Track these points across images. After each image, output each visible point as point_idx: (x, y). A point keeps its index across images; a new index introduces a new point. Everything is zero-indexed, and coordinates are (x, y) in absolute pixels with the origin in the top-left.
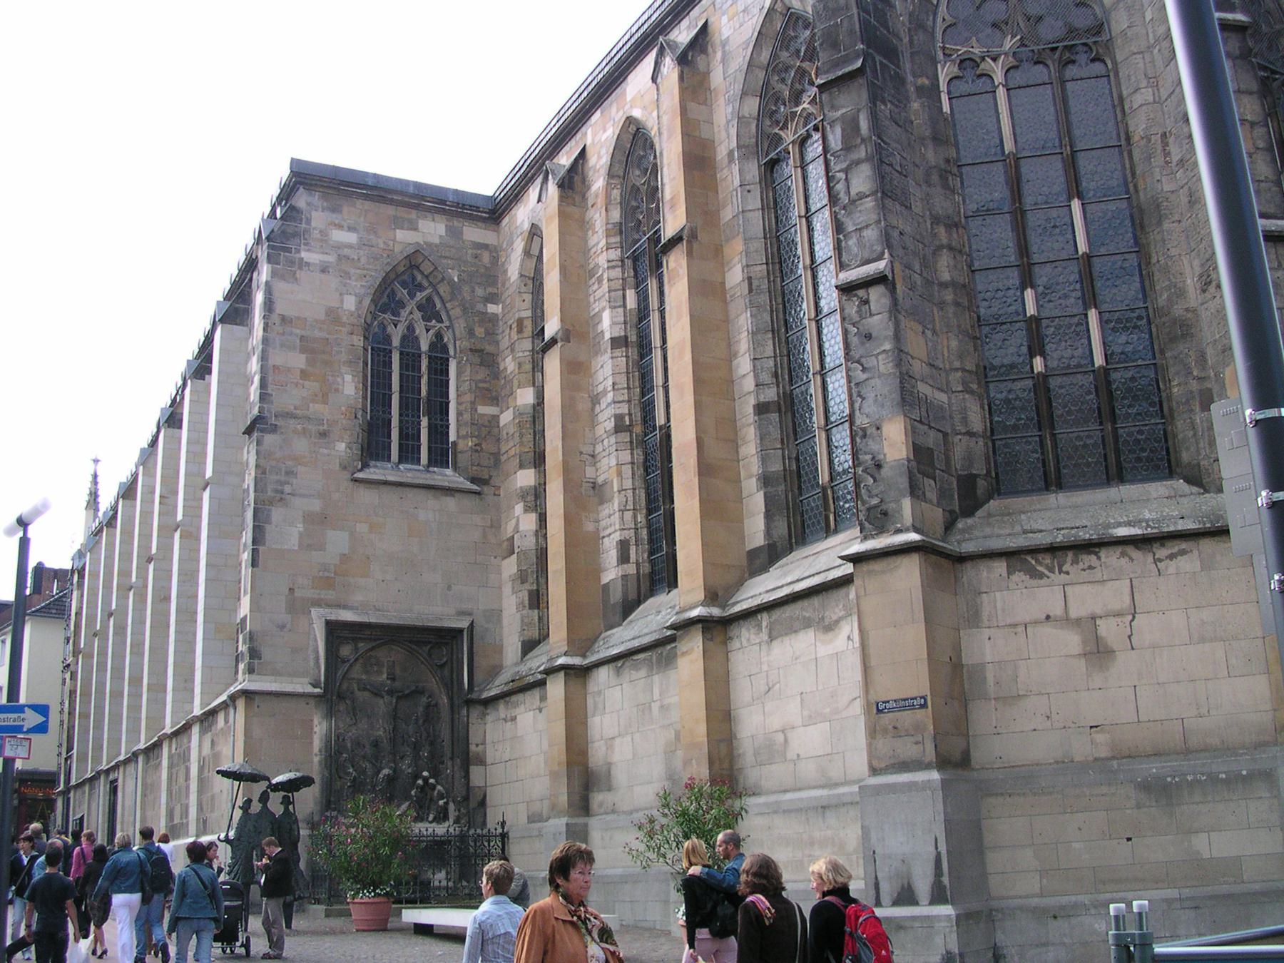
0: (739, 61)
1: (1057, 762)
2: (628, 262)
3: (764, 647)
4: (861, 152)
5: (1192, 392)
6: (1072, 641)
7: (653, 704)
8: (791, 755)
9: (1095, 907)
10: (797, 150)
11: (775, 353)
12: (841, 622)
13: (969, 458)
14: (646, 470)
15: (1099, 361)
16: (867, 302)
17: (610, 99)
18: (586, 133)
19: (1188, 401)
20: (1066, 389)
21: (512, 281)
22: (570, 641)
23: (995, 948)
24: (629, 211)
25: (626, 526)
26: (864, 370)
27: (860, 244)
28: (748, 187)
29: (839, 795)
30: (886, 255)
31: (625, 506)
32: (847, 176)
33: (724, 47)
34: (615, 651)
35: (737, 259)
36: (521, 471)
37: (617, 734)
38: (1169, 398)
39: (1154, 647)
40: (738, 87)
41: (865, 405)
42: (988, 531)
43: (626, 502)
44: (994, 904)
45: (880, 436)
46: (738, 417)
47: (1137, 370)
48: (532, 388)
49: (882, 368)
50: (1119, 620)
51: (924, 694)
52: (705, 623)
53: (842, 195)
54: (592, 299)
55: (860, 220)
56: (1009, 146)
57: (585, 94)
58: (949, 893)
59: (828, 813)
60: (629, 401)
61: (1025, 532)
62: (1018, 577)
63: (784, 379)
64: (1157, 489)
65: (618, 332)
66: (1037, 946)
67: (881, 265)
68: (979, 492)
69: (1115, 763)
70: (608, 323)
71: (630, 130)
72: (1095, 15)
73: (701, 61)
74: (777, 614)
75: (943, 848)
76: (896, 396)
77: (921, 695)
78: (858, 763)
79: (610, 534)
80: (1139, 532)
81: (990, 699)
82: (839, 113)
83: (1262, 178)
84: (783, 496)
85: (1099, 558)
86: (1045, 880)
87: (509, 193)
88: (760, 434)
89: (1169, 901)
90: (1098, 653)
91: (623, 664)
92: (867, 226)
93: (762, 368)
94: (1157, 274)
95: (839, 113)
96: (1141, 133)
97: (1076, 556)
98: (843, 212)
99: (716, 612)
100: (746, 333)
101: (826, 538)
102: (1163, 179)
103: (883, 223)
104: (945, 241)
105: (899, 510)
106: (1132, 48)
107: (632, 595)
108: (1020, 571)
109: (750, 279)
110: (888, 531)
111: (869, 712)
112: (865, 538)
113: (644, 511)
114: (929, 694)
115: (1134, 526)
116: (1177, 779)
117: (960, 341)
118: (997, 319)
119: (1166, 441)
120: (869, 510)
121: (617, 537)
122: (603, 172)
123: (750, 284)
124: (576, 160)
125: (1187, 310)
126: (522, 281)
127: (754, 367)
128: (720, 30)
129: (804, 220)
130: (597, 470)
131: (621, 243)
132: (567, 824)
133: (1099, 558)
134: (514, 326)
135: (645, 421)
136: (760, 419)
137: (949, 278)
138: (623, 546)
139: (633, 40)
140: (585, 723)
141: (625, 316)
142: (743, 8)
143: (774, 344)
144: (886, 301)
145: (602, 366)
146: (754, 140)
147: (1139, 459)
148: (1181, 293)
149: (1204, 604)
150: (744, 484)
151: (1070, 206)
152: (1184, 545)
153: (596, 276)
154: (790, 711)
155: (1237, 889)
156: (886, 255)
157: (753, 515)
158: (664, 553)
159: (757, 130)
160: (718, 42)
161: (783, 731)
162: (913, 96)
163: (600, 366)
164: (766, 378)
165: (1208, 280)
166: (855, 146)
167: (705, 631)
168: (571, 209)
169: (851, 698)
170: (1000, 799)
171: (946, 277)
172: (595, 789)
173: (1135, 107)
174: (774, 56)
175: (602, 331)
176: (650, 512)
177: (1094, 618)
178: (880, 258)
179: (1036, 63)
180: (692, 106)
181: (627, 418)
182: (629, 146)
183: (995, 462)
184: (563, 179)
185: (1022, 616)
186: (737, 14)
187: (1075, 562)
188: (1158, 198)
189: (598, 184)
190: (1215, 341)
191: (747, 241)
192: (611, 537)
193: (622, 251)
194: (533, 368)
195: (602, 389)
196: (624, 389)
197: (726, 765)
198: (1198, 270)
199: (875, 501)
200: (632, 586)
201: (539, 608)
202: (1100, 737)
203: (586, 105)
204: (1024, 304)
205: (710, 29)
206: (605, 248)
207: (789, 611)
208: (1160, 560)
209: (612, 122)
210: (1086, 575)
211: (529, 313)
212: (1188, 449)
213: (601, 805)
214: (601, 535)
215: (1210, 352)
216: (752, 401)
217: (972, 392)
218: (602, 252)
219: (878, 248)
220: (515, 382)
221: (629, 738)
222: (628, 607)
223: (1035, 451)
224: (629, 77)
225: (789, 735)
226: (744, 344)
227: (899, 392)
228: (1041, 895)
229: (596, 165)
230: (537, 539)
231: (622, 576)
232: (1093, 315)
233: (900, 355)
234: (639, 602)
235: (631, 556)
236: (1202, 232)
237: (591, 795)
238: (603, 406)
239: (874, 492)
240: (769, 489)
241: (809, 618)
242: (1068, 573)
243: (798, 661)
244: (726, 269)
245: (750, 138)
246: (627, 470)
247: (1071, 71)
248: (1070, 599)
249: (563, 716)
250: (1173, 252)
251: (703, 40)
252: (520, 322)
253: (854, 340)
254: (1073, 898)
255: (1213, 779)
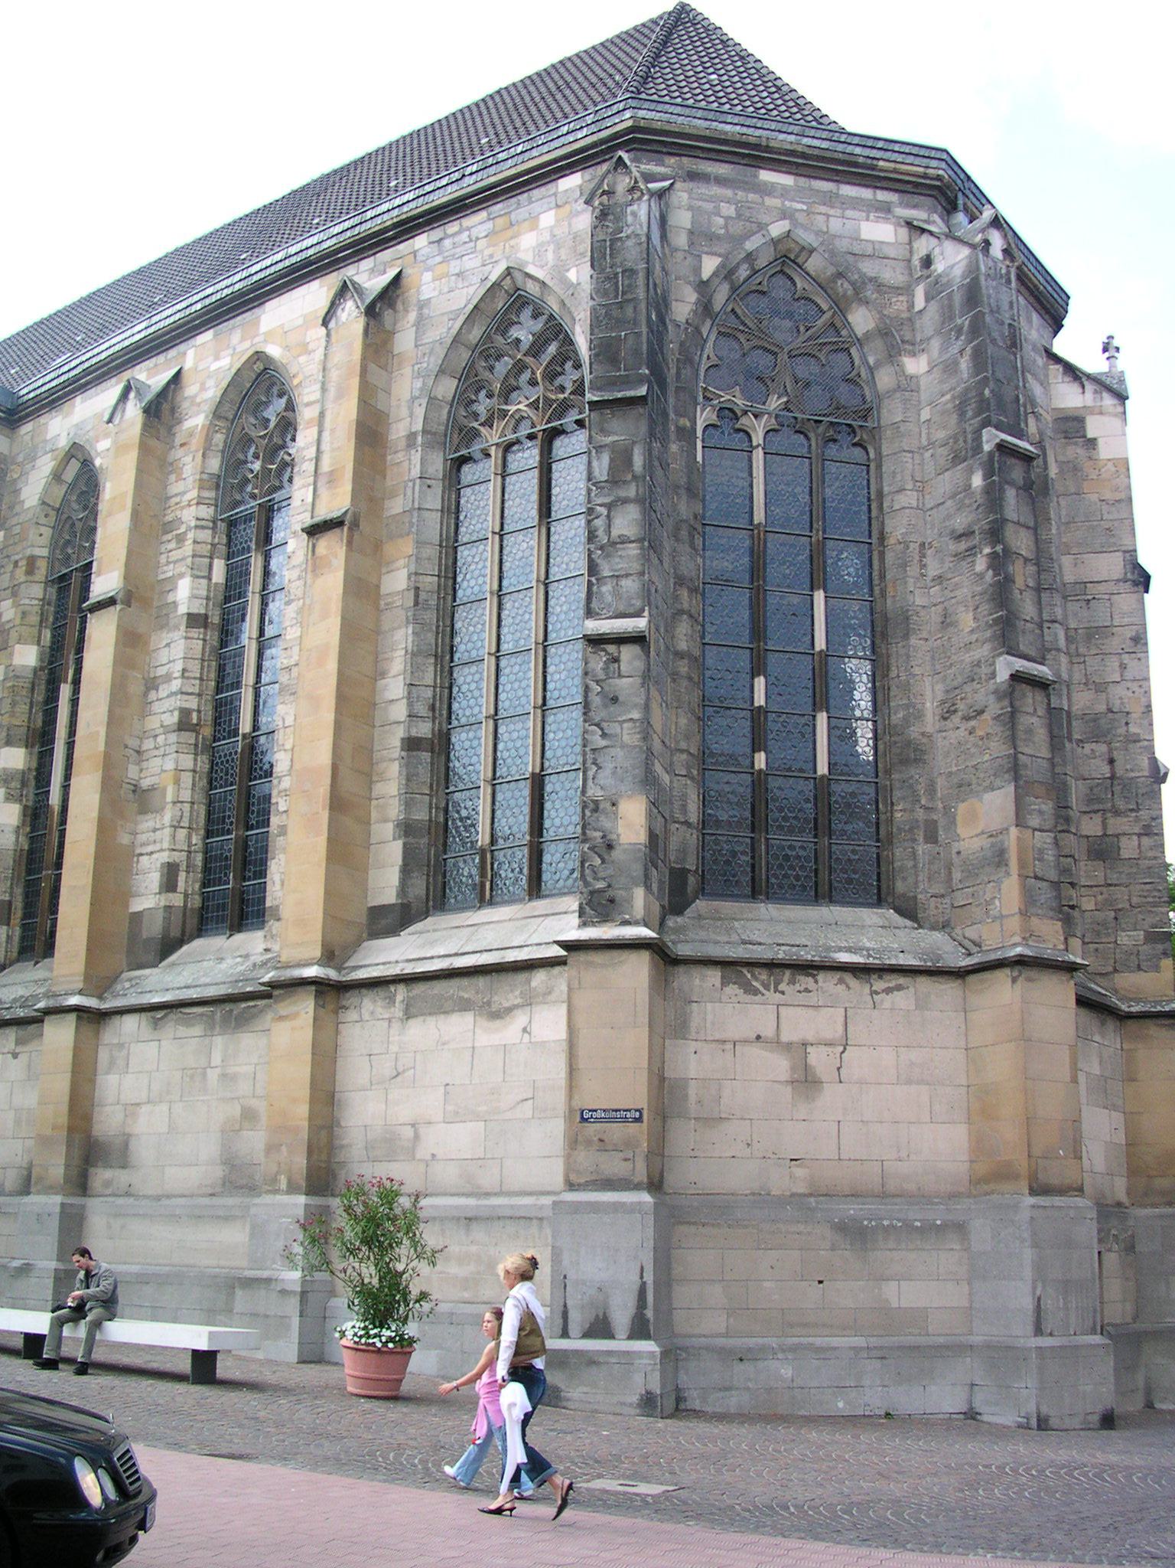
0: (442, 331)
1: (753, 1194)
2: (221, 526)
3: (396, 1025)
4: (631, 491)
5: (917, 821)
6: (781, 1066)
7: (209, 1070)
8: (422, 1153)
9: (783, 1351)
10: (500, 455)
11: (435, 682)
12: (515, 1011)
13: (683, 851)
14: (210, 783)
15: (822, 769)
16: (616, 660)
17: (232, 322)
18: (185, 354)
19: (911, 829)
20: (788, 791)
21: (27, 505)
22: (87, 977)
23: (677, 1389)
24: (234, 464)
25: (177, 847)
26: (604, 735)
27: (616, 593)
28: (429, 482)
29: (494, 1207)
30: (646, 613)
31: (179, 822)
32: (609, 512)
33: (421, 308)
34: (156, 999)
35: (402, 562)
36: (7, 748)
37: (145, 1100)
38: (890, 820)
39: (861, 1082)
40: (434, 362)
41: (601, 775)
42: (703, 934)
43: (181, 817)
44: (679, 1341)
45: (615, 814)
46: (376, 747)
47: (858, 785)
48: (35, 647)
49: (626, 738)
50: (830, 1049)
51: (640, 1107)
52: (321, 987)
53: (600, 533)
54: (163, 559)
55: (620, 566)
56: (759, 516)
57: (199, 306)
58: (651, 1328)
59: (474, 1226)
60: (200, 695)
61: (744, 942)
62: (732, 989)
63: (441, 715)
64: (870, 916)
65: (198, 608)
66: (720, 1390)
67: (641, 623)
68: (689, 889)
69: (812, 1200)
70: (185, 595)
71: (255, 367)
72: (863, 396)
73: (388, 316)
74: (420, 989)
75: (649, 1278)
76: (639, 772)
77: (636, 1107)
78: (553, 1174)
79: (152, 853)
80: (861, 960)
81: (690, 1119)
82: (610, 439)
83: (1028, 618)
84: (425, 851)
85: (816, 982)
86: (731, 1320)
87: (44, 396)
88: (407, 775)
89: (856, 1350)
90: (806, 1082)
91: (165, 1016)
92: (627, 575)
93: (418, 697)
94: (893, 688)
95: (610, 439)
96: (899, 537)
97: (793, 975)
98: (600, 552)
99: (332, 974)
100: (403, 652)
101: (479, 908)
102: (917, 592)
103: (647, 576)
104: (686, 606)
105: (630, 900)
106: (903, 444)
107: (175, 932)
108: (735, 983)
109: (417, 589)
110: (613, 921)
111: (570, 1118)
112: (584, 925)
113: (202, 832)
114: (645, 1107)
115: (855, 953)
116: (873, 1223)
117: (689, 720)
118: (722, 702)
119: (879, 866)
120: (592, 893)
121: (165, 857)
122: (208, 408)
123: (417, 596)
124: (169, 383)
125: (923, 734)
126: (43, 510)
127: (409, 693)
128: (419, 288)
129: (497, 537)
130: (141, 770)
131: (216, 500)
132: (63, 1205)
133: (816, 982)
134: (24, 562)
135: (216, 722)
136: (409, 757)
137: (686, 648)
138: (170, 872)
139: (287, 263)
140: (92, 1081)
141: (209, 590)
142: (457, 271)
143: (436, 671)
144: (639, 665)
145: (168, 645)
146: (443, 428)
147: (850, 881)
148: (920, 715)
149: (914, 1044)
150: (375, 828)
151: (812, 596)
152: (902, 980)
153: (175, 533)
154: (429, 1103)
155: (922, 1340)
156: (646, 613)
157: (383, 867)
158: (230, 886)
159: (449, 417)
160: (413, 300)
161: (413, 1125)
162: (673, 437)
163: (164, 643)
164: (422, 710)
165: (952, 708)
166: (625, 482)
167: (319, 995)
168: (153, 443)
169: (521, 1097)
170: (693, 1229)
171: (683, 646)
172: (100, 1164)
173: (896, 507)
174: (487, 337)
175: (174, 602)
176: (209, 834)
177: (805, 1045)
178: (638, 614)
179: (796, 432)
180: (372, 367)
181: (195, 715)
182: (248, 386)
183: (703, 858)
184: (151, 403)
185: (733, 1032)
186: (447, 275)
187: (792, 982)
188: (908, 610)
189: (195, 420)
190: (951, 773)
191: (420, 544)
192: (155, 856)
193: (216, 511)
194: (41, 621)
195: (164, 673)
196: (195, 678)
197: (324, 1157)
198: (940, 696)
199: (600, 885)
200: (176, 919)
201: (8, 924)
202: (799, 1172)
203: (194, 320)
204: (752, 691)
205: (405, 281)
206: (195, 502)
207: (439, 987)
208: (877, 993)
209: (230, 351)
210: (802, 998)
211: (45, 552)
212: (904, 879)
213: (107, 1184)
214: (138, 851)
215: (940, 782)
216: (400, 733)
217: (692, 779)
218: (189, 505)
219: (638, 603)
220: (14, 635)
221: (165, 1107)
222: (168, 946)
223: (744, 853)
224: (268, 304)
225: (422, 1130)
226: (397, 662)
227: (643, 770)
228: (727, 1335)
229: (196, 396)
230: (17, 838)
231: (165, 907)
232: (822, 719)
233: (646, 728)
234: (181, 942)
235: (179, 884)
236: (953, 657)
237: (92, 1170)
238: (162, 693)
239: (601, 874)
240: (411, 840)
241: (468, 1001)
242: (783, 993)
243: (446, 1047)
244: (384, 570)
245: (439, 425)
246: (187, 779)
247: (832, 450)
248: (782, 1020)
249: (69, 1068)
250: (917, 670)
251: (394, 292)
252: (32, 561)
253: (596, 701)
254: (760, 1341)
255: (908, 1226)
